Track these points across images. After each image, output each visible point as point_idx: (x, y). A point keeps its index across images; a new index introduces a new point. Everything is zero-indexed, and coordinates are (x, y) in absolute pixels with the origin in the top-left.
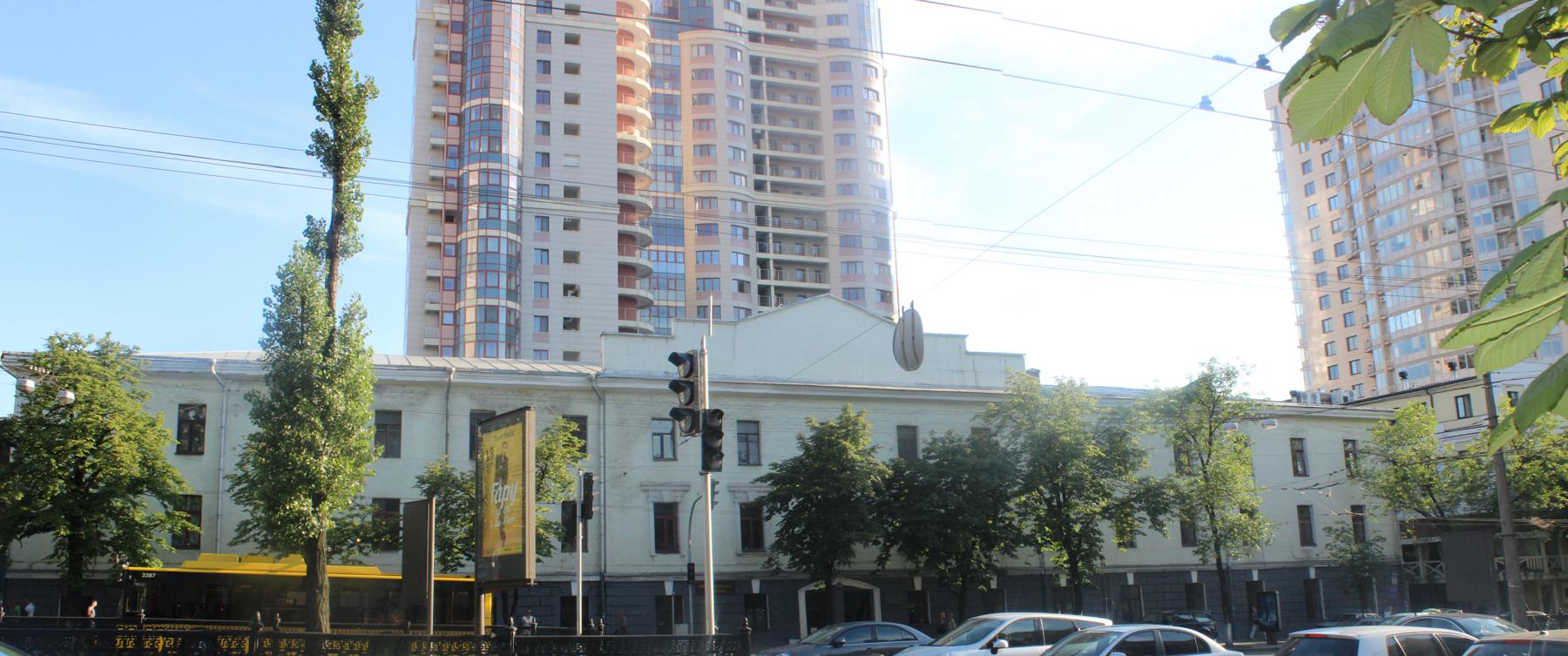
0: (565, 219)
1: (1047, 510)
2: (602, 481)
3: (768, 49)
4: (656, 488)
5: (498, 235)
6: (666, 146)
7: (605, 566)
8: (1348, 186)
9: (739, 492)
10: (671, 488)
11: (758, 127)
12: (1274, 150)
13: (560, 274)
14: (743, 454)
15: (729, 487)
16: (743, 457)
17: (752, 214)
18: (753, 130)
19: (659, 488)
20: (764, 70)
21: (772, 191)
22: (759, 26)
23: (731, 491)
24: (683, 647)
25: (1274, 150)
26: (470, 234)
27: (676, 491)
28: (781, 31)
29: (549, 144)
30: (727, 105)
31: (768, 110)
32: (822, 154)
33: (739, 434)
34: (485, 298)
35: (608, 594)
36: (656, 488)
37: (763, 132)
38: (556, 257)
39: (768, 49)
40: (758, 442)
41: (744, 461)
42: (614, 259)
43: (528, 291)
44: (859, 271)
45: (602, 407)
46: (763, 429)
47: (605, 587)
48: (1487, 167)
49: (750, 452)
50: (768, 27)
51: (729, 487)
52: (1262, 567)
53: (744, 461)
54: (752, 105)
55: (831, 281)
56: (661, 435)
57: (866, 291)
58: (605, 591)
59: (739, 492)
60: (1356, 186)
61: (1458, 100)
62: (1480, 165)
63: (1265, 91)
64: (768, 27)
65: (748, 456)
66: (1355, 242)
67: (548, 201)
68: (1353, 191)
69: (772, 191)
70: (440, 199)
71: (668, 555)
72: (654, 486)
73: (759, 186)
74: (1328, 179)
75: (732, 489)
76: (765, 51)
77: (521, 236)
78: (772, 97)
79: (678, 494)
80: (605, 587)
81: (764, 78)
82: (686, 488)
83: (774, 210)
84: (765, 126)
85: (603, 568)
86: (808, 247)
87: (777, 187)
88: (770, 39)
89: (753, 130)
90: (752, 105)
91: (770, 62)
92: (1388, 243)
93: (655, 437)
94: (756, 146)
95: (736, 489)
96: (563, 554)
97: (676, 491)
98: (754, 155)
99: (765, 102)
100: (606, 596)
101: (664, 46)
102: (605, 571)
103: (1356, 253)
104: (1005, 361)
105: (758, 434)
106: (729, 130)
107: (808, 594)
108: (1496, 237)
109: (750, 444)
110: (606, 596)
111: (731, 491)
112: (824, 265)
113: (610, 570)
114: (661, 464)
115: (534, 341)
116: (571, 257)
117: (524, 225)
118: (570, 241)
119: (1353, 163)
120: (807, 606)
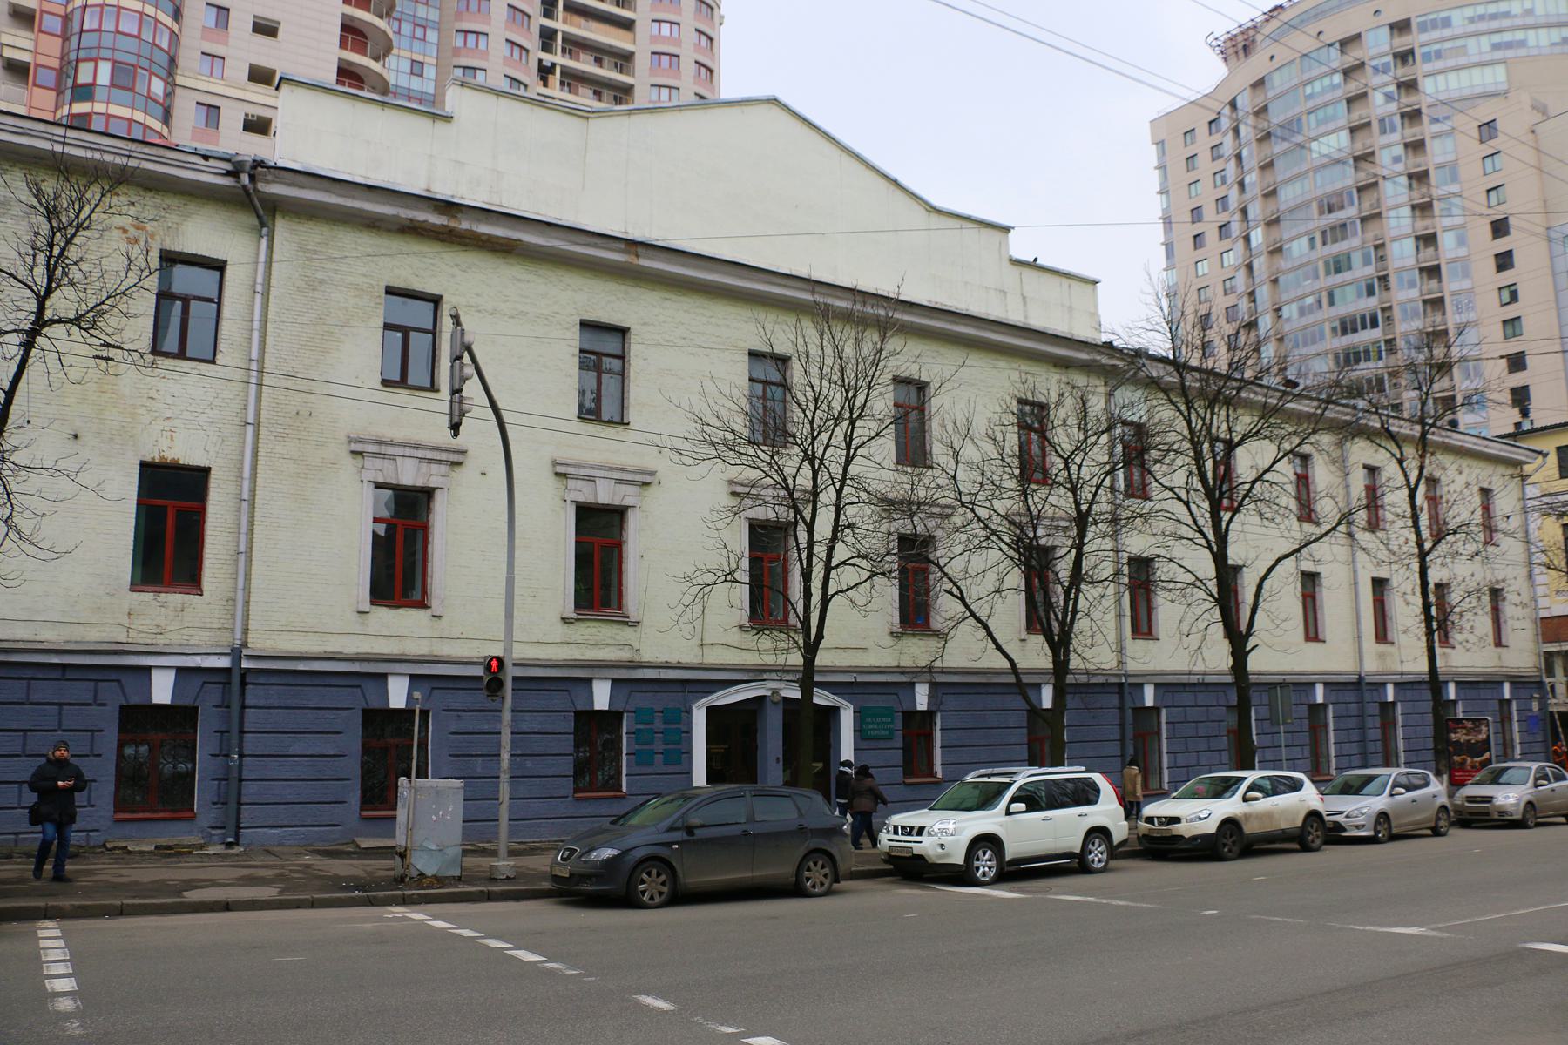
0: (247, 115)
2: (250, 420)
4: (384, 449)
5: (129, 116)
7: (246, 631)
8: (1247, 239)
9: (577, 477)
10: (420, 453)
11: (548, 58)
12: (1158, 193)
14: (589, 397)
15: (555, 463)
16: (588, 404)
18: (540, 61)
19: (390, 450)
23: (557, 474)
24: (1, 288)
25: (1158, 193)
27: (430, 461)
33: (581, 351)
35: (248, 702)
36: (384, 449)
37: (553, 65)
40: (622, 374)
41: (589, 412)
45: (264, 242)
46: (635, 349)
47: (243, 684)
48: (1414, 222)
49: (603, 392)
51: (555, 463)
52: (1398, 678)
53: (589, 412)
56: (406, 331)
58: (243, 693)
59: (577, 477)
60: (1257, 236)
61: (1384, 140)
62: (1409, 244)
63: (1151, 122)
65: (598, 399)
66: (1252, 304)
67: (220, 82)
68: (1254, 244)
71: (401, 611)
72: (379, 443)
74: (1223, 228)
75: (560, 469)
77: (167, 126)
79: (434, 468)
80: (243, 684)
82: (455, 457)
84: (558, 58)
85: (238, 635)
89: (540, 61)
90: (542, 26)
92: (1294, 306)
93: (389, 333)
94: (542, 83)
95: (570, 470)
96: (135, 595)
97: (430, 461)
100: (243, 707)
102: (245, 645)
103: (1253, 318)
104: (1070, 286)
105: (622, 357)
106: (508, 53)
107: (712, 712)
108: (1420, 304)
109: (604, 376)
110: (243, 707)
111: (557, 474)
113: (259, 642)
114: (400, 397)
117: (177, 113)
119: (1255, 211)
120: (689, 732)
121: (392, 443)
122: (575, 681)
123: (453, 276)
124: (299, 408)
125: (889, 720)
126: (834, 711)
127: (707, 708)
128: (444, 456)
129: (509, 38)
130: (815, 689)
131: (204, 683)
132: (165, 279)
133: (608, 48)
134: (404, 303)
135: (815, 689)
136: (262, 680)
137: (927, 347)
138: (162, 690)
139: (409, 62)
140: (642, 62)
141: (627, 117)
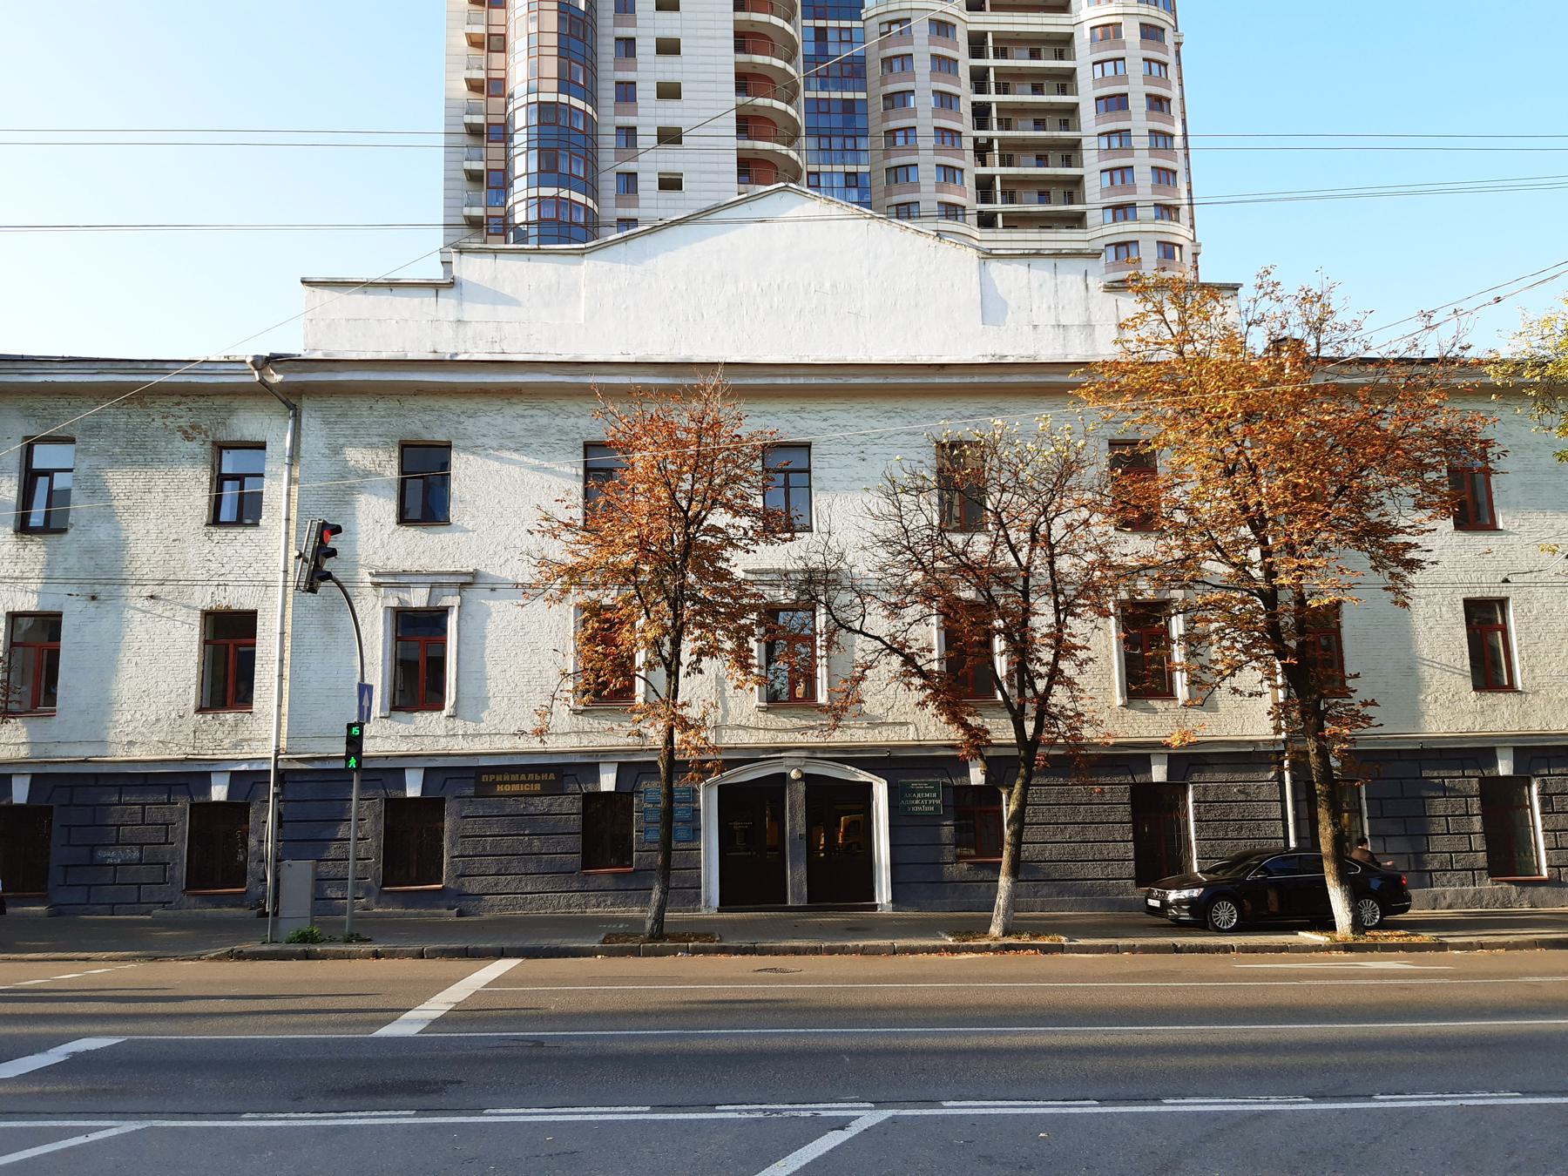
3: (995, 19)
6: (847, 174)
20: (999, 194)
21: (1004, 227)
26: (517, 197)
29: (635, 26)
30: (933, 106)
31: (1004, 218)
32: (1082, 166)
34: (539, 235)
37: (990, 140)
39: (995, 19)
42: (728, 98)
44: (1134, 256)
54: (974, 104)
78: (1005, 124)
86: (1056, 193)
87: (1013, 221)
89: (976, 140)
99: (995, 169)
101: (841, 29)
107: (724, 791)
112: (1078, 181)
121: (405, 573)
122: (588, 767)
123: (460, 423)
124: (524, 529)
125: (935, 795)
126: (868, 787)
127: (720, 787)
128: (452, 579)
129: (937, 126)
130: (1015, 741)
131: (254, 783)
132: (217, 464)
133: (1048, 107)
134: (1066, 357)
135: (1015, 741)
136: (298, 778)
137: (979, 406)
138: (219, 792)
139: (844, 175)
140: (1087, 112)
141: (623, 244)
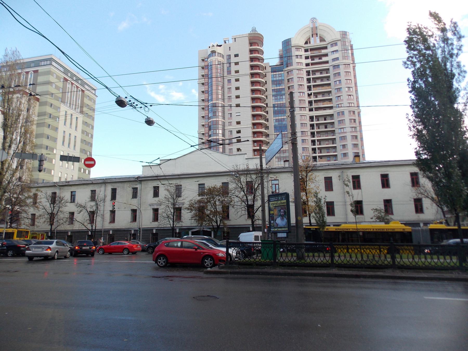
1: (398, 253)
13: (234, 93)
17: (308, 118)
18: (308, 93)
21: (315, 111)
22: (309, 61)
28: (317, 60)
31: (312, 71)
38: (233, 89)
43: (227, 116)
50: (312, 60)
55: (338, 160)
57: (347, 137)
64: (312, 60)
69: (315, 111)
70: (204, 130)
73: (311, 110)
76: (314, 113)
81: (311, 76)
83: (316, 116)
84: (315, 122)
86: (325, 79)
88: (312, 64)
89: (308, 93)
91: (313, 71)
98: (309, 101)
115: (228, 120)
116: (237, 88)
118: (237, 84)
